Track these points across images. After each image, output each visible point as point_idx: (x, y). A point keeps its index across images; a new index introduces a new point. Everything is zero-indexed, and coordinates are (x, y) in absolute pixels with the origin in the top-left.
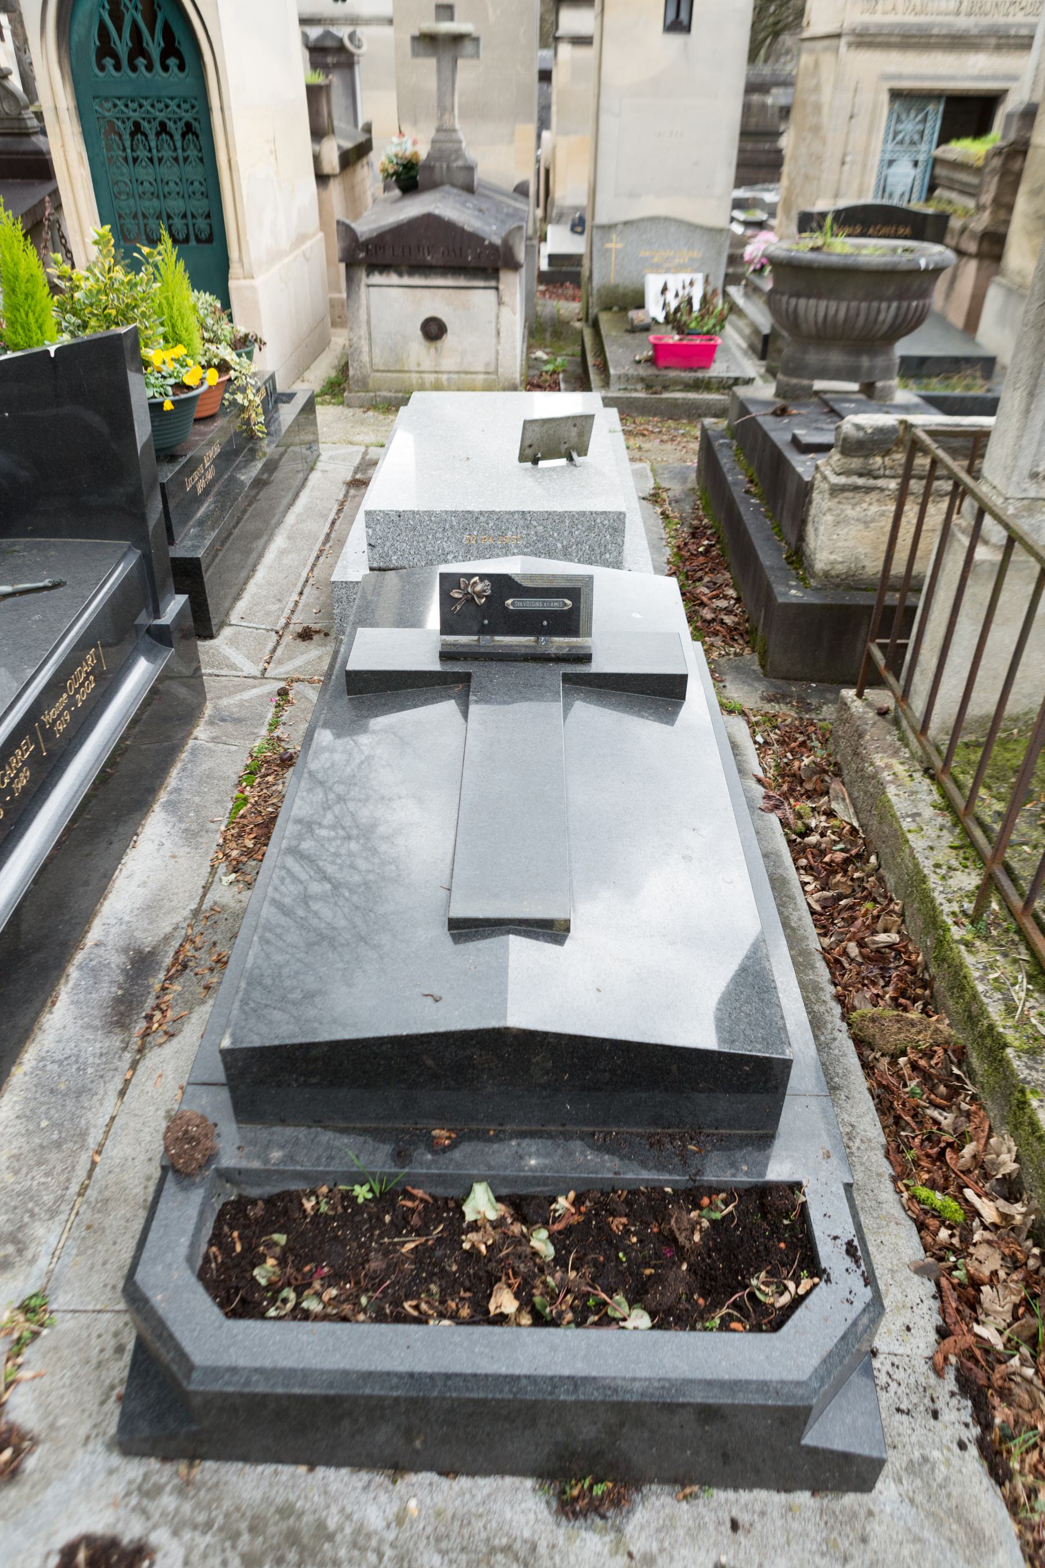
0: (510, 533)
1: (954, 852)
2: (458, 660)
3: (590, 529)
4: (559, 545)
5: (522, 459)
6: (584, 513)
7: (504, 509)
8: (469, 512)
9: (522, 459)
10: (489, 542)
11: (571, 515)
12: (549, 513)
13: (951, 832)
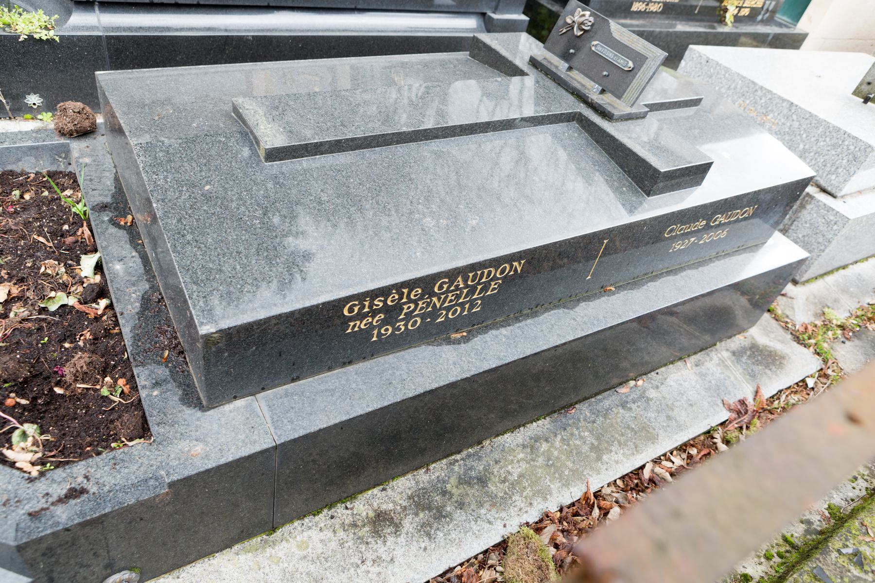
0: (771, 116)
1: (781, 541)
2: (537, 68)
3: (834, 146)
4: (801, 146)
5: (857, 92)
6: (839, 130)
7: (779, 94)
8: (753, 83)
9: (857, 92)
10: (753, 114)
11: (827, 125)
12: (811, 115)
13: (807, 532)
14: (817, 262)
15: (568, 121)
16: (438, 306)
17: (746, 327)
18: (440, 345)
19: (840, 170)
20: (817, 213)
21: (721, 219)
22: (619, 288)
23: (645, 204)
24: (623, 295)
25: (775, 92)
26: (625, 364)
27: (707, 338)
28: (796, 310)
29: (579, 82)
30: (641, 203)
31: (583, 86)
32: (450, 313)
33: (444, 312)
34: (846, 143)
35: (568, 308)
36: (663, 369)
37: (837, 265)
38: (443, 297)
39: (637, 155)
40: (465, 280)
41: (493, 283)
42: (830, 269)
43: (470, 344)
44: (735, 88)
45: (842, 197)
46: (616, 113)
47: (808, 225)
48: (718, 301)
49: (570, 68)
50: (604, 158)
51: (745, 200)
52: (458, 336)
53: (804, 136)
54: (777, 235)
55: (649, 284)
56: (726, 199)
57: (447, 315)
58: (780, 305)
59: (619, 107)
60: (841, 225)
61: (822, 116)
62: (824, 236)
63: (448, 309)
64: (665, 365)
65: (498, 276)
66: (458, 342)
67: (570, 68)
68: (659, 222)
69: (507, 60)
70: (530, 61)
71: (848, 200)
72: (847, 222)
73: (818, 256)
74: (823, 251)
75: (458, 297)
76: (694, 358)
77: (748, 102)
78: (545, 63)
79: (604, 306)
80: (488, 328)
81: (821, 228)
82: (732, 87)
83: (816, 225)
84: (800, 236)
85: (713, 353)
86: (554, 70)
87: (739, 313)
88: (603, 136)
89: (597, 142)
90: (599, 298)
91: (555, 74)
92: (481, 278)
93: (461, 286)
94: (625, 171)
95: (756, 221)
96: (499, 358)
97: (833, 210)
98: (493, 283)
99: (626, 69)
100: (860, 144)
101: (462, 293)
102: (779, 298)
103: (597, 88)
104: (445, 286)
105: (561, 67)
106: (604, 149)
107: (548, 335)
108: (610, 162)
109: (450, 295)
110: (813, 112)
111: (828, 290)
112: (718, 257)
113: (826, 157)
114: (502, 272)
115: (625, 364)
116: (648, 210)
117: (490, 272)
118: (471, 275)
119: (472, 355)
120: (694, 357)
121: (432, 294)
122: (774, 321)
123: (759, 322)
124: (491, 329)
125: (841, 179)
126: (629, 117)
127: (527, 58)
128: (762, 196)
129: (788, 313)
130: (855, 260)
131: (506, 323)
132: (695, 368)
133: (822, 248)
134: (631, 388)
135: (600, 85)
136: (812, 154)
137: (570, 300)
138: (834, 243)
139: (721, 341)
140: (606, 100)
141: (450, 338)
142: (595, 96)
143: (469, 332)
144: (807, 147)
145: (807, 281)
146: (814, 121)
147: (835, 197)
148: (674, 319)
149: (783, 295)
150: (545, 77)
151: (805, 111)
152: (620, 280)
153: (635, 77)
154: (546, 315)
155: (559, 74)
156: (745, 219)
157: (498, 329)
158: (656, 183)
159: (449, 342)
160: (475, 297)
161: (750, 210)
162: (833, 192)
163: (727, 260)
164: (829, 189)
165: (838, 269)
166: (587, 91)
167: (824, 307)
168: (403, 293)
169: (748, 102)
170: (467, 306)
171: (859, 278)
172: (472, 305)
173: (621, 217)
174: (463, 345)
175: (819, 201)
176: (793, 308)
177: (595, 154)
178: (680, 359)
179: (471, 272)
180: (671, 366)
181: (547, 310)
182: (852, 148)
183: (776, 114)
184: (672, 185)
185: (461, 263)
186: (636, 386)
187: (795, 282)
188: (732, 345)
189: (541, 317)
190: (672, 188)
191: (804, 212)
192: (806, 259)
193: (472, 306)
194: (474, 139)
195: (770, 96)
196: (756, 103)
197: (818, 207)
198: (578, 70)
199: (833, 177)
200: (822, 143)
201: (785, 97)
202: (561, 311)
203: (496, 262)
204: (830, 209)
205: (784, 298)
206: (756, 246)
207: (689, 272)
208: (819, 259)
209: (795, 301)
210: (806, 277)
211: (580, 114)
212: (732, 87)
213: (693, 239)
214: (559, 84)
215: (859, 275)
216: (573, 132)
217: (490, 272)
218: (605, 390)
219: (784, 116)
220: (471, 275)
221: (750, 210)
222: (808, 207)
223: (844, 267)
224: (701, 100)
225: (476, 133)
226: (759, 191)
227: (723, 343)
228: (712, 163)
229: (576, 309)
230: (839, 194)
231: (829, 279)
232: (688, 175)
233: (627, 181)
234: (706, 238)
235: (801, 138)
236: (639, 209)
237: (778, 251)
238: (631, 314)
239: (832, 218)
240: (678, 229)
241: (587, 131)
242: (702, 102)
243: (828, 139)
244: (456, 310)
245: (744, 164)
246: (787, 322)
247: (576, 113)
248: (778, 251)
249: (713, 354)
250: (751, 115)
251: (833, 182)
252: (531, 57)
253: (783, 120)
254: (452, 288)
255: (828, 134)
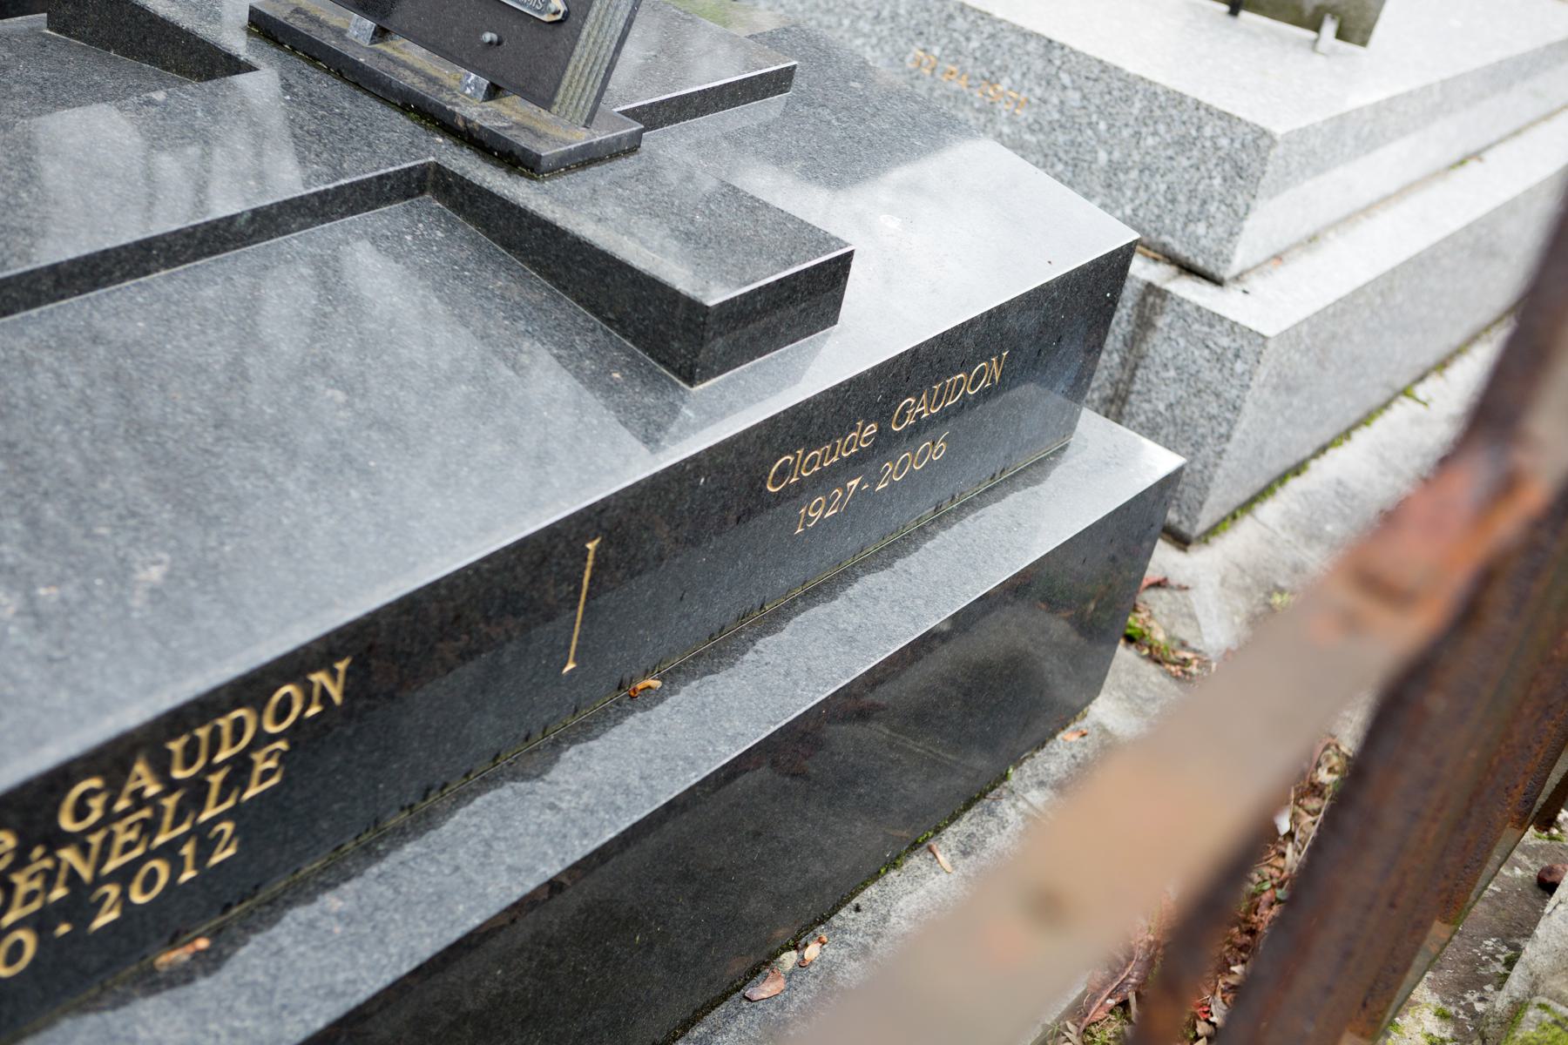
0: (1005, 83)
2: (278, 44)
3: (1183, 144)
4: (1103, 157)
10: (959, 85)
11: (1152, 92)
12: (1105, 68)
14: (1220, 472)
15: (408, 196)
16: (86, 873)
17: (1077, 703)
18: (122, 1001)
19: (1212, 208)
20: (1186, 333)
21: (918, 407)
22: (674, 677)
23: (687, 412)
24: (687, 696)
25: (998, 15)
26: (755, 906)
27: (981, 761)
28: (1202, 620)
29: (416, 72)
30: (674, 411)
31: (431, 80)
32: (163, 879)
33: (113, 891)
34: (1208, 131)
35: (527, 777)
36: (872, 891)
37: (1277, 467)
38: (95, 839)
39: (631, 269)
40: (161, 768)
41: (257, 757)
42: (1260, 482)
43: (226, 974)
44: (894, 16)
45: (1237, 278)
46: (546, 151)
47: (1172, 373)
48: (990, 641)
49: (381, 34)
50: (538, 291)
51: (968, 342)
52: (181, 955)
53: (1102, 126)
54: (1091, 425)
55: (760, 645)
56: (915, 351)
57: (124, 895)
58: (1156, 616)
59: (555, 133)
60: (1251, 358)
61: (1132, 66)
62: (1218, 395)
63: (124, 876)
64: (875, 876)
65: (271, 728)
66: (183, 976)
67: (381, 34)
68: (741, 454)
69: (176, 29)
70: (252, 22)
71: (1254, 282)
72: (1264, 345)
73: (1220, 454)
74: (1228, 438)
75: (149, 828)
76: (952, 835)
77: (936, 51)
78: (299, 24)
79: (637, 742)
80: (275, 908)
81: (1206, 375)
82: (885, 13)
83: (1193, 369)
84: (1161, 407)
85: (1005, 803)
86: (333, 43)
87: (1052, 666)
88: (520, 226)
89: (508, 246)
90: (617, 722)
91: (338, 54)
92: (215, 746)
93: (152, 790)
94: (608, 321)
95: (1027, 391)
96: (332, 993)
97: (1222, 319)
98: (257, 757)
99: (546, 18)
100: (1240, 129)
101: (159, 811)
102: (1149, 596)
103: (474, 82)
104: (96, 804)
105: (352, 33)
106: (534, 265)
107: (480, 879)
108: (557, 300)
109: (119, 827)
110: (1107, 59)
111: (1270, 542)
112: (942, 519)
113: (1170, 177)
114: (281, 715)
115: (755, 906)
116: (696, 428)
117: (239, 726)
118: (176, 746)
119: (241, 1005)
120: (952, 829)
121: (61, 839)
122: (1151, 668)
123: (1109, 680)
124: (289, 904)
125: (1220, 231)
126: (588, 158)
127: (245, 15)
128: (1011, 322)
129: (1183, 633)
130: (1318, 443)
131: (335, 874)
132: (960, 863)
133: (1223, 430)
134: (790, 976)
135: (479, 72)
136: (1134, 174)
137: (528, 750)
138: (1248, 408)
139: (1017, 762)
140: (506, 116)
141: (153, 970)
142: (474, 110)
143: (215, 934)
144: (1116, 155)
145: (1214, 530)
146: (1116, 84)
147: (1217, 282)
148: (876, 731)
149: (1160, 585)
150: (308, 69)
151: (1088, 58)
152: (672, 652)
153: (576, 38)
154: (460, 816)
155: (350, 52)
156: (986, 394)
157: (311, 898)
158: (702, 341)
159: (154, 983)
160: (204, 817)
161: (993, 368)
162: (1211, 268)
163: (969, 520)
164: (1200, 262)
165: (1282, 479)
166: (446, 97)
167: (1269, 594)
168: (169, 753)
169: (936, 51)
170: (188, 850)
171: (1341, 490)
172: (205, 840)
173: (637, 464)
174: (203, 983)
175: (1181, 302)
176: (1192, 617)
177: (507, 281)
178: (915, 846)
179: (174, 736)
180: (893, 874)
181: (463, 798)
182: (1224, 142)
183: (1017, 76)
184: (752, 339)
185: (134, 715)
186: (802, 964)
187: (1181, 541)
188: (1053, 768)
189: (447, 828)
190: (755, 348)
191: (1155, 338)
192: (1180, 470)
193: (206, 846)
194: (107, 304)
195: (988, 29)
196: (958, 52)
197: (1183, 317)
198: (407, 35)
199: (1201, 229)
200: (1150, 141)
201: (1030, 25)
202: (506, 791)
203: (251, 689)
204: (1214, 319)
205: (1164, 593)
206: (1040, 462)
207: (870, 581)
208: (1225, 463)
209: (1193, 596)
210: (1205, 521)
211: (439, 169)
212: (885, 13)
213: (855, 483)
214: (357, 85)
215: (1340, 482)
216: (428, 227)
217: (239, 726)
218: (712, 1005)
219: (1039, 77)
220: (176, 746)
221: (993, 368)
222: (1161, 322)
223: (1298, 469)
224: (789, 73)
225: (111, 282)
226: (1000, 309)
227: (1026, 767)
228: (850, 255)
229: (554, 775)
230: (1227, 274)
231: (1268, 511)
232: (791, 301)
233: (621, 348)
234: (891, 472)
235: (1095, 131)
236: (673, 429)
237: (1105, 466)
238: (723, 748)
239: (1225, 342)
240: (804, 463)
241: (470, 218)
242: (797, 80)
243: (1162, 128)
244: (153, 874)
245: (933, 251)
246: (1185, 662)
247: (424, 169)
248: (1105, 466)
249: (1006, 809)
250: (955, 86)
251: (1203, 242)
252: (253, 12)
253: (1038, 91)
254: (122, 804)
255: (1158, 113)
